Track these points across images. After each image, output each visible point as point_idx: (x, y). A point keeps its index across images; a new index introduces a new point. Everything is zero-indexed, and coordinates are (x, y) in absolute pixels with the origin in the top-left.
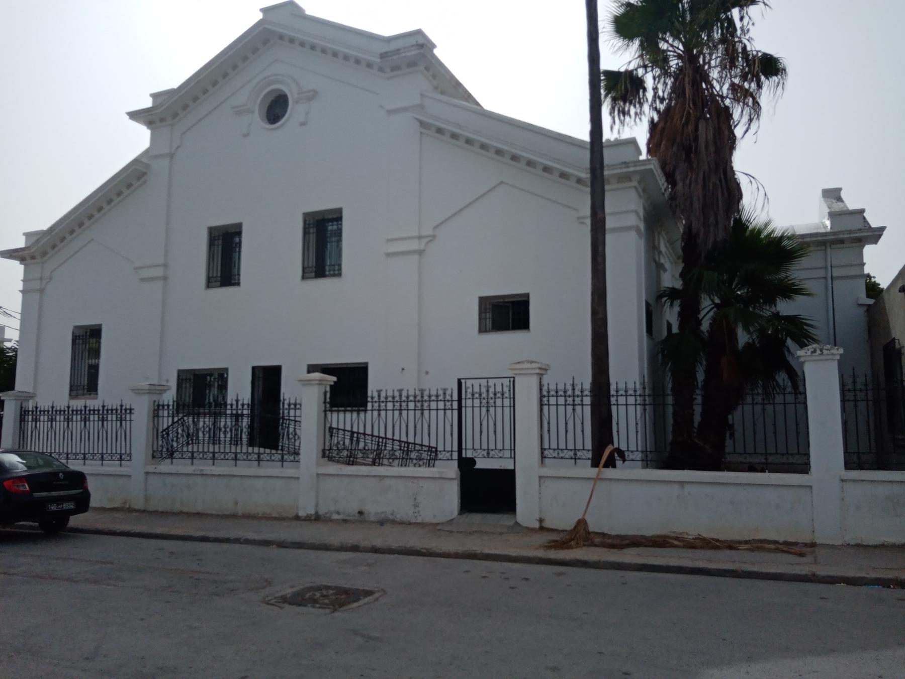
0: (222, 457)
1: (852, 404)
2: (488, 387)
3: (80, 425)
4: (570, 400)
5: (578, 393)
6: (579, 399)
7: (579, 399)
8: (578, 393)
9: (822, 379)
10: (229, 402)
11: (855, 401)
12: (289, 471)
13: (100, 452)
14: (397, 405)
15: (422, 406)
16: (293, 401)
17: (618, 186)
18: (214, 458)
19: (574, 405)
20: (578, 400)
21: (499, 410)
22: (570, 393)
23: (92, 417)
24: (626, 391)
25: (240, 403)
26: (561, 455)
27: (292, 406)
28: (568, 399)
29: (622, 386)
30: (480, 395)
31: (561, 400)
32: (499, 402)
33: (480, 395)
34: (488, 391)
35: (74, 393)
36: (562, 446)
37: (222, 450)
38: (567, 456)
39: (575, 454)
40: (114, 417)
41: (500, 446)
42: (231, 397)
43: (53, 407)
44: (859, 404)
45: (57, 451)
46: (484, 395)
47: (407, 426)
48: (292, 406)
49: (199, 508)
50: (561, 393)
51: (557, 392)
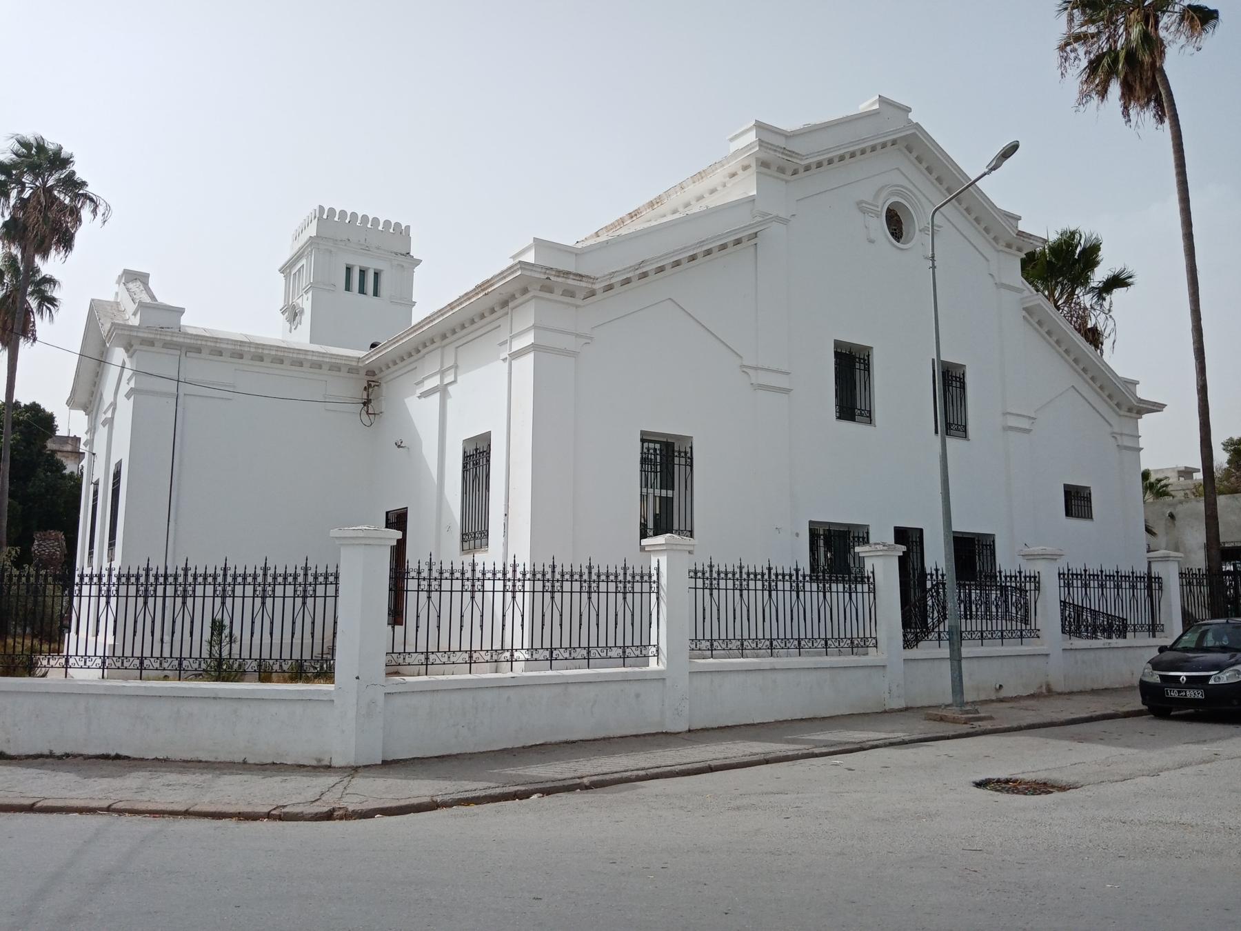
2: (474, 565)
4: (424, 584)
5: (435, 574)
7: (426, 583)
8: (435, 574)
10: (928, 571)
12: (1028, 647)
13: (823, 636)
14: (548, 584)
16: (240, 571)
18: (982, 638)
19: (429, 591)
22: (425, 574)
23: (780, 584)
25: (773, 571)
26: (452, 659)
27: (240, 580)
28: (422, 582)
33: (544, 575)
34: (514, 571)
35: (466, 546)
36: (731, 636)
39: (471, 657)
40: (787, 585)
41: (444, 647)
42: (929, 566)
43: (1020, 572)
45: (753, 636)
47: (272, 623)
48: (240, 580)
49: (1107, 684)
50: (457, 575)
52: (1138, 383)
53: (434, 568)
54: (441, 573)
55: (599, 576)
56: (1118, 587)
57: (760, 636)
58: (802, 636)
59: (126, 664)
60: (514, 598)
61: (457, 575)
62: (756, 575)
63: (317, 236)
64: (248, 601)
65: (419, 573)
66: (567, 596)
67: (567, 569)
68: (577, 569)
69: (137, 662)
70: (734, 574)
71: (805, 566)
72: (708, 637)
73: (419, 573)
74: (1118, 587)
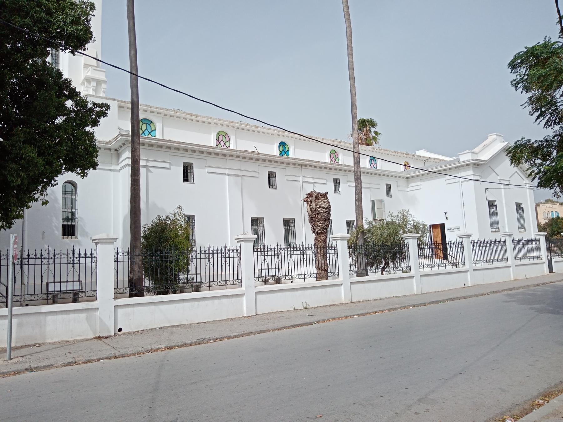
0: (216, 284)
1: (46, 266)
3: (489, 248)
4: (45, 261)
6: (77, 259)
7: (46, 260)
9: (412, 245)
11: (48, 264)
15: (209, 256)
17: (148, 148)
20: (51, 261)
21: (296, 256)
24: (123, 253)
28: (44, 260)
29: (32, 252)
30: (205, 251)
31: (38, 261)
32: (231, 255)
33: (205, 251)
37: (270, 274)
38: (41, 299)
44: (50, 266)
46: (207, 252)
50: (219, 252)
51: (201, 252)
52: (327, 193)
53: (76, 253)
54: (79, 255)
55: (196, 252)
56: (491, 246)
57: (300, 273)
58: (306, 273)
59: (219, 284)
60: (209, 261)
61: (219, 252)
62: (271, 249)
63: (88, 169)
64: (299, 256)
65: (91, 255)
66: (215, 260)
67: (269, 247)
68: (203, 249)
69: (303, 276)
70: (274, 249)
71: (282, 244)
72: (303, 273)
73: (91, 255)
74: (491, 246)
